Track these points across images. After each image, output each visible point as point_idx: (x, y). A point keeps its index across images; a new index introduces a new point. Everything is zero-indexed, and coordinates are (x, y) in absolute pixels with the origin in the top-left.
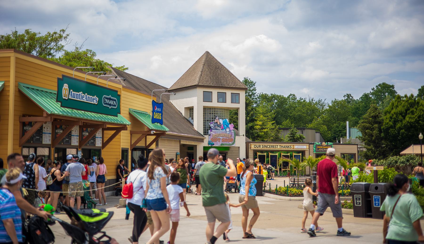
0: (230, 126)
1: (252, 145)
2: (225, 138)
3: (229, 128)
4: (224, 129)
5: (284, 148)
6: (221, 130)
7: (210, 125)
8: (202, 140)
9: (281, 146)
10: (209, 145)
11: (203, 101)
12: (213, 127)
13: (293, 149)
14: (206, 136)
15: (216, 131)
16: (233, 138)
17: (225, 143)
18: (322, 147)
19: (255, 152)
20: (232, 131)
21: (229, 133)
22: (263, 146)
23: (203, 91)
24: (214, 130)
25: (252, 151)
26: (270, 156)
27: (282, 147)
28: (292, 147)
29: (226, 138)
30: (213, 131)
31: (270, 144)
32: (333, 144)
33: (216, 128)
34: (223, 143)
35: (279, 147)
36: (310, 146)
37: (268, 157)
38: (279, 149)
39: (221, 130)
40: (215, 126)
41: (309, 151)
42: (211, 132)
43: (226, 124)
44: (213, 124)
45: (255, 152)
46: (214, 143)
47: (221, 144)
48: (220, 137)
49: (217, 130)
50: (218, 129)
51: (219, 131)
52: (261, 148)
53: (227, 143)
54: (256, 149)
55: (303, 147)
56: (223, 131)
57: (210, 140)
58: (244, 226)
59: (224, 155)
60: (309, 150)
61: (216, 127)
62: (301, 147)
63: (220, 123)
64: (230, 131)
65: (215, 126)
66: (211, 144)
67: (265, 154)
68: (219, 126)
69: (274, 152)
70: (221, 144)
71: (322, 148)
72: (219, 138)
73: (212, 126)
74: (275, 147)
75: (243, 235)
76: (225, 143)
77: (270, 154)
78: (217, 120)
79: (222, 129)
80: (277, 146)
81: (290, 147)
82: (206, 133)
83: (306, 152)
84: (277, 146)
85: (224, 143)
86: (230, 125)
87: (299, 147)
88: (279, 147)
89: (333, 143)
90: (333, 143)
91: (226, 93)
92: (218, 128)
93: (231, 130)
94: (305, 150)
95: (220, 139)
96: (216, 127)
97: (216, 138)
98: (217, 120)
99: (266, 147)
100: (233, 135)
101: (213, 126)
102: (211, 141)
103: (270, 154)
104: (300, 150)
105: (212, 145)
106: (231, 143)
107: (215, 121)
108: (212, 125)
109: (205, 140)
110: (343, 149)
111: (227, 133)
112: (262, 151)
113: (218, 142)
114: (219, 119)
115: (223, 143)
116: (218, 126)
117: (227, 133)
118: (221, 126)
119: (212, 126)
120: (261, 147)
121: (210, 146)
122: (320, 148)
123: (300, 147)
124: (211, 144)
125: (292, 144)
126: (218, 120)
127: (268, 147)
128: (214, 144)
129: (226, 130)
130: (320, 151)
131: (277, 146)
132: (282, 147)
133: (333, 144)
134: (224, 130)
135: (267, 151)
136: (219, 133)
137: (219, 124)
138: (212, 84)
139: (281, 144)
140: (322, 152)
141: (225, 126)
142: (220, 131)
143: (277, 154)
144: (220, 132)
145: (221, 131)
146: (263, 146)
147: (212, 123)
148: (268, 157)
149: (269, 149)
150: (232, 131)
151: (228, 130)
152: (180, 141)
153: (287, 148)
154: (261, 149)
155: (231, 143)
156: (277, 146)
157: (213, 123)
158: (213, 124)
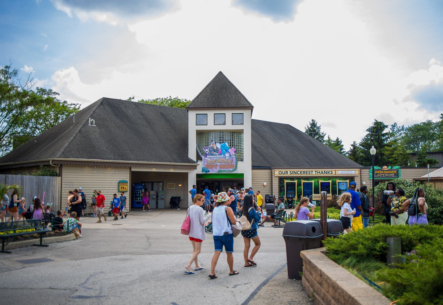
0: (230, 150)
1: (276, 172)
2: (223, 164)
3: (230, 153)
4: (223, 154)
5: (322, 174)
6: (219, 155)
7: (205, 150)
8: (195, 167)
9: (317, 172)
10: (203, 172)
11: (196, 125)
12: (208, 152)
13: (335, 174)
14: (199, 162)
15: (212, 156)
16: (235, 164)
17: (224, 169)
18: (382, 172)
19: (281, 180)
20: (233, 156)
21: (229, 158)
22: (292, 172)
23: (196, 114)
24: (209, 155)
25: (277, 178)
26: (302, 184)
27: (319, 173)
28: (334, 172)
29: (225, 164)
30: (208, 156)
31: (302, 170)
32: (400, 168)
33: (212, 153)
34: (221, 169)
35: (314, 173)
36: (362, 171)
37: (299, 184)
38: (315, 175)
39: (219, 155)
40: (211, 151)
41: (361, 177)
42: (206, 158)
43: (226, 148)
44: (208, 149)
45: (281, 180)
46: (209, 169)
47: (219, 171)
48: (217, 163)
49: (214, 155)
50: (215, 155)
51: (216, 156)
52: (289, 174)
53: (227, 169)
54: (282, 175)
55: (350, 172)
56: (221, 156)
57: (205, 167)
58: (246, 255)
59: (354, 186)
60: (361, 175)
61: (212, 152)
62: (347, 172)
63: (217, 148)
64: (230, 155)
65: (211, 151)
66: (206, 171)
67: (296, 181)
68: (217, 150)
69: (310, 179)
70: (218, 170)
71: (382, 173)
72: (215, 164)
73: (207, 152)
74: (308, 173)
75: (244, 263)
76: (224, 169)
77: (303, 181)
78: (213, 144)
79: (221, 154)
80: (312, 172)
81: (330, 172)
82: (199, 158)
83: (355, 178)
84: (312, 172)
85: (222, 170)
86: (230, 149)
87: (344, 172)
88: (314, 173)
89: (400, 167)
90: (400, 167)
91: (225, 114)
92: (215, 153)
93: (231, 154)
94: (354, 176)
95: (217, 165)
96: (212, 152)
97: (212, 164)
98: (213, 144)
99: (296, 174)
100: (234, 160)
101: (208, 151)
102: (206, 168)
103: (303, 181)
104: (347, 176)
105: (207, 172)
106: (231, 169)
107: (211, 146)
108: (207, 150)
109: (198, 167)
110: (410, 176)
111: (227, 158)
112: (292, 178)
113: (214, 168)
114: (215, 143)
115: (221, 169)
116: (215, 151)
117: (227, 158)
118: (218, 151)
119: (206, 151)
120: (289, 173)
121: (204, 173)
122: (379, 174)
123: (345, 172)
124: (206, 171)
125: (333, 170)
126: (215, 144)
127: (299, 173)
128: (209, 171)
129: (224, 155)
130: (379, 176)
131: (311, 172)
132: (319, 173)
133: (400, 168)
134: (223, 155)
135: (299, 178)
136: (215, 158)
137: (216, 149)
138: (206, 106)
139: (317, 170)
140: (383, 177)
141: (224, 151)
142: (217, 157)
143: (313, 181)
144: (218, 158)
145: (218, 156)
146: (292, 172)
147: (207, 148)
148: (299, 184)
149: (299, 176)
150: (233, 156)
151: (227, 155)
152: (130, 168)
153: (326, 173)
154: (289, 176)
155: (231, 169)
156: (311, 172)
157: (209, 148)
158: (208, 149)
